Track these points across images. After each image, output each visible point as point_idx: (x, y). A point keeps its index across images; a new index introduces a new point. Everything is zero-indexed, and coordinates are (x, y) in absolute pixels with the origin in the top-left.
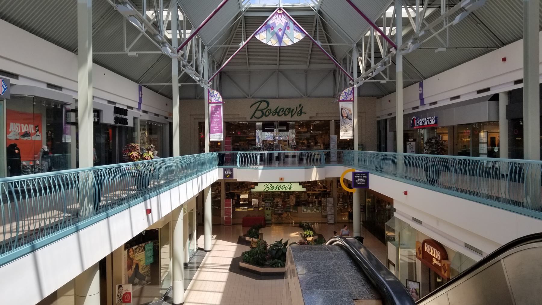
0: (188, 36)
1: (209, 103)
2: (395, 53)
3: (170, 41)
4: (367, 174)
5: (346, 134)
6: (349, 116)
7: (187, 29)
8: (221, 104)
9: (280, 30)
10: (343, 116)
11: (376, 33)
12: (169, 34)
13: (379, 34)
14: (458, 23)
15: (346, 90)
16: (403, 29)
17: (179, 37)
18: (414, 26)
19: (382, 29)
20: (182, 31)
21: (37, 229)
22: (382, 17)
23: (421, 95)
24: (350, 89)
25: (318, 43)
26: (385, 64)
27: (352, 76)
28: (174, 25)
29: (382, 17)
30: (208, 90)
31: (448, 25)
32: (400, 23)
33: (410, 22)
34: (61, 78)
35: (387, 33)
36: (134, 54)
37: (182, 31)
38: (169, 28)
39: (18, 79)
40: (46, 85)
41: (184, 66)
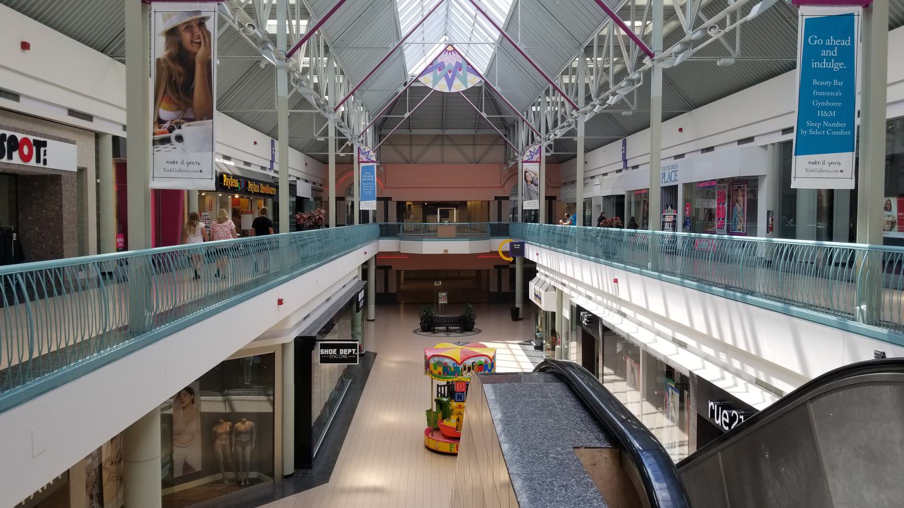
0: (303, 31)
1: (359, 162)
2: (650, 65)
3: (273, 38)
4: (522, 245)
5: (530, 205)
6: (535, 180)
7: (302, 19)
8: (375, 164)
9: (450, 72)
10: (527, 181)
11: (618, 31)
12: (272, 26)
13: (623, 32)
14: (756, 18)
15: (532, 149)
16: (665, 24)
17: (288, 32)
18: (685, 22)
19: (628, 24)
20: (294, 22)
21: (16, 367)
22: (630, 3)
23: (624, 155)
24: (537, 147)
25: (484, 115)
26: (632, 82)
27: (540, 130)
28: (280, 13)
29: (630, 3)
30: (359, 148)
31: (740, 22)
32: (659, 14)
33: (675, 13)
34: (17, 76)
35: (637, 32)
36: (343, 155)
37: (294, 22)
38: (273, 16)
39: (92, 121)
40: (66, 112)
41: (297, 81)
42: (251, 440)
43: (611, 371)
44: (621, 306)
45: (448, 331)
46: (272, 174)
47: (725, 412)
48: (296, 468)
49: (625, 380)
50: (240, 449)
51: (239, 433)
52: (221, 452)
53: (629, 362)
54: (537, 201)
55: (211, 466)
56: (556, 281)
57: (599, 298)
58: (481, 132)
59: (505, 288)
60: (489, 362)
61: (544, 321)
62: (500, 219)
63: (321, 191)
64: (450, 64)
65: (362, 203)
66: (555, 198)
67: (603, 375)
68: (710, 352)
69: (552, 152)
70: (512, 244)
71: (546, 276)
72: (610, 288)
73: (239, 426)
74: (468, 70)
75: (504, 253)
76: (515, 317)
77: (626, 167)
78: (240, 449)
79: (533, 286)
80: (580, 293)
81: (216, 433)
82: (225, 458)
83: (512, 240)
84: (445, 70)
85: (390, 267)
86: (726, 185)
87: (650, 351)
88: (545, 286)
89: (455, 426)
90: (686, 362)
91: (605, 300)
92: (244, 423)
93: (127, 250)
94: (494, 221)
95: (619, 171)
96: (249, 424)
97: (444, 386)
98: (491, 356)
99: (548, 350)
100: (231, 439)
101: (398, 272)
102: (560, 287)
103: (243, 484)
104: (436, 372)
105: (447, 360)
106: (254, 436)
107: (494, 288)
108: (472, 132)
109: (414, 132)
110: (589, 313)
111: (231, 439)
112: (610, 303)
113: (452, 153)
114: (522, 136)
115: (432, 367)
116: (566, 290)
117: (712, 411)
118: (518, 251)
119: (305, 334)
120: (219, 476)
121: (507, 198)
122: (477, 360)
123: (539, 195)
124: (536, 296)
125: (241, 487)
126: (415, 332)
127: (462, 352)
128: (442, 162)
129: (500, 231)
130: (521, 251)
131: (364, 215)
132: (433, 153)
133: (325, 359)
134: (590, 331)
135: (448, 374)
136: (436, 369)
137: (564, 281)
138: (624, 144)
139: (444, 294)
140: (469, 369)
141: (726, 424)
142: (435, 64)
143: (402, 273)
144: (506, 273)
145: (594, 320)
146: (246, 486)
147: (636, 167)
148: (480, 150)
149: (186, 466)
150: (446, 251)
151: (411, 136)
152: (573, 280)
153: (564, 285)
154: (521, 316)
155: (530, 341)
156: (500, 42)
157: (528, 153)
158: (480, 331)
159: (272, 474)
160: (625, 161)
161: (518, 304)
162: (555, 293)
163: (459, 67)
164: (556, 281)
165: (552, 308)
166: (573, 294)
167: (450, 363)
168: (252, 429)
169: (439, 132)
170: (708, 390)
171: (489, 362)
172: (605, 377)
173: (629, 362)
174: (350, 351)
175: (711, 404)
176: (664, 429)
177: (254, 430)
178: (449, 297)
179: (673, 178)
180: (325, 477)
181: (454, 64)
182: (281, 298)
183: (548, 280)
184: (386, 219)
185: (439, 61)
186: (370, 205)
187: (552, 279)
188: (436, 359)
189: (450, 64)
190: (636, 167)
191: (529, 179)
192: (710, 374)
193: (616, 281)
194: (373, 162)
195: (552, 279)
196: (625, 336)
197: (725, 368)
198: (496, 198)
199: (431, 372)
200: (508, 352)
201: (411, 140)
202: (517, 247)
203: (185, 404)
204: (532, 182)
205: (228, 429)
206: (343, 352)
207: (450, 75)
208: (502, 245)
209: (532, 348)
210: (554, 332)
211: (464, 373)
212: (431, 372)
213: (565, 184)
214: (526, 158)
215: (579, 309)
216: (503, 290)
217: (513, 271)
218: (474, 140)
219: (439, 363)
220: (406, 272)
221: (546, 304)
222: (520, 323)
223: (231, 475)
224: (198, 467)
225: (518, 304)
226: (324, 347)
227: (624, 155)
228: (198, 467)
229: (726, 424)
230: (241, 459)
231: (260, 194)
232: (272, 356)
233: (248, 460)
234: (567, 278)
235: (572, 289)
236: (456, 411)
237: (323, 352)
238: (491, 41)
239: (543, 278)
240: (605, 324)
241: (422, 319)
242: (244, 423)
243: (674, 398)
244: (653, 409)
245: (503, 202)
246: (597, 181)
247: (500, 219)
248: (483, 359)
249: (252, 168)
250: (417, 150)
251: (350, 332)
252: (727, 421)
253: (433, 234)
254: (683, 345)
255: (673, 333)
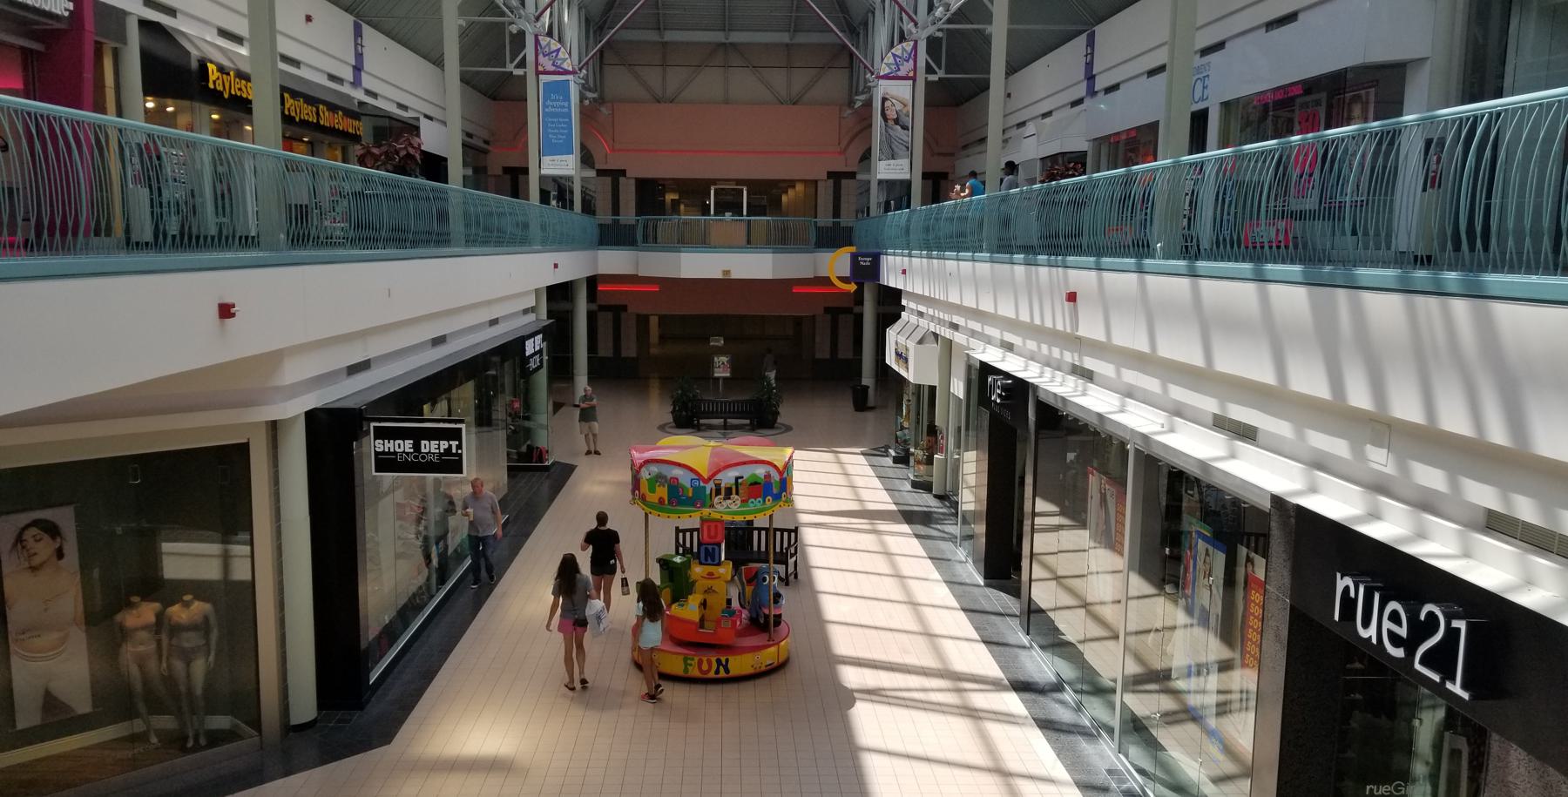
1: (538, 73)
4: (876, 259)
5: (887, 169)
15: (898, 50)
23: (1089, 65)
24: (908, 46)
42: (208, 644)
43: (1052, 508)
44: (1082, 360)
45: (725, 427)
46: (359, 95)
47: (1393, 605)
48: (321, 705)
49: (1083, 525)
50: (179, 665)
51: (176, 630)
52: (134, 670)
53: (1095, 482)
54: (905, 162)
55: (116, 700)
56: (940, 322)
57: (1032, 345)
58: (802, 38)
59: (845, 353)
60: (776, 477)
61: (913, 408)
62: (836, 213)
63: (485, 152)
65: (546, 160)
66: (944, 176)
67: (1034, 514)
68: (1338, 447)
69: (941, 74)
70: (854, 257)
71: (921, 314)
72: (1058, 319)
73: (177, 613)
75: (842, 279)
76: (861, 404)
77: (1092, 92)
78: (179, 665)
79: (892, 335)
80: (988, 340)
81: (122, 628)
82: (145, 682)
83: (853, 249)
85: (624, 308)
86: (1323, 96)
87: (1157, 452)
88: (918, 335)
89: (696, 618)
90: (1262, 474)
91: (1045, 348)
92: (187, 605)
94: (825, 219)
95: (1079, 102)
96: (199, 608)
97: (692, 531)
98: (780, 465)
99: (919, 462)
100: (159, 642)
101: (643, 321)
102: (946, 333)
103: (190, 744)
104: (653, 498)
105: (677, 472)
106: (214, 636)
107: (823, 352)
108: (784, 38)
109: (670, 36)
110: (1007, 375)
111: (159, 642)
112: (1056, 352)
113: (744, 83)
114: (881, 36)
115: (644, 488)
116: (959, 338)
117: (1349, 604)
118: (866, 271)
120: (138, 726)
121: (852, 175)
122: (747, 472)
123: (909, 149)
124: (899, 355)
125: (184, 750)
126: (662, 428)
127: (715, 453)
128: (726, 102)
129: (832, 238)
130: (874, 271)
131: (557, 191)
132: (709, 83)
133: (387, 463)
134: (1007, 415)
135: (679, 503)
136: (652, 490)
137: (956, 319)
138: (1091, 43)
139: (724, 359)
140: (729, 492)
141: (1395, 640)
143: (654, 321)
144: (846, 321)
145: (1019, 389)
146: (197, 748)
147: (1114, 88)
148: (800, 78)
149: (50, 703)
150: (727, 272)
151: (664, 44)
152: (977, 314)
153: (955, 327)
154: (871, 402)
155: (887, 447)
157: (889, 59)
158: (788, 429)
159: (256, 723)
160: (1090, 78)
161: (867, 380)
162: (934, 349)
164: (940, 322)
165: (931, 378)
166: (974, 342)
167: (685, 478)
168: (206, 618)
169: (718, 37)
170: (1324, 545)
171: (776, 477)
172: (1038, 520)
173: (1095, 482)
174: (444, 445)
175: (1343, 582)
176: (1179, 633)
177: (213, 620)
178: (734, 366)
179: (1197, 96)
180: (385, 732)
182: (228, 300)
183: (923, 322)
184: (616, 210)
186: (563, 165)
187: (932, 318)
188: (654, 469)
190: (1114, 88)
191: (892, 114)
192: (1335, 503)
193: (1072, 297)
194: (566, 72)
195: (932, 318)
196: (1094, 421)
197: (1378, 487)
198: (831, 175)
199: (643, 498)
200: (835, 468)
201: (666, 54)
202: (865, 262)
203: (37, 561)
204: (897, 121)
205: (152, 619)
206: (430, 447)
208: (836, 264)
209: (889, 461)
210: (932, 430)
211: (716, 500)
212: (643, 498)
213: (965, 147)
214: (885, 70)
215: (986, 369)
216: (841, 356)
217: (859, 318)
218: (789, 55)
219: (659, 478)
220: (663, 319)
221: (917, 370)
222: (869, 415)
223: (166, 722)
224: (82, 704)
225: (867, 380)
226: (382, 434)
227: (1089, 65)
228: (82, 704)
229: (1395, 640)
230: (183, 688)
231: (332, 131)
232: (243, 450)
233: (199, 691)
234: (965, 311)
235: (973, 334)
236: (701, 585)
237: (382, 446)
239: (914, 319)
240: (1042, 397)
241: (674, 404)
242: (187, 605)
243: (1207, 561)
244: (1148, 589)
245: (844, 182)
246: (1030, 129)
247: (836, 213)
248: (760, 471)
249: (303, 72)
250: (675, 77)
251: (1136, 594)
252: (1403, 632)
253: (701, 241)
254: (1246, 433)
255: (1223, 407)
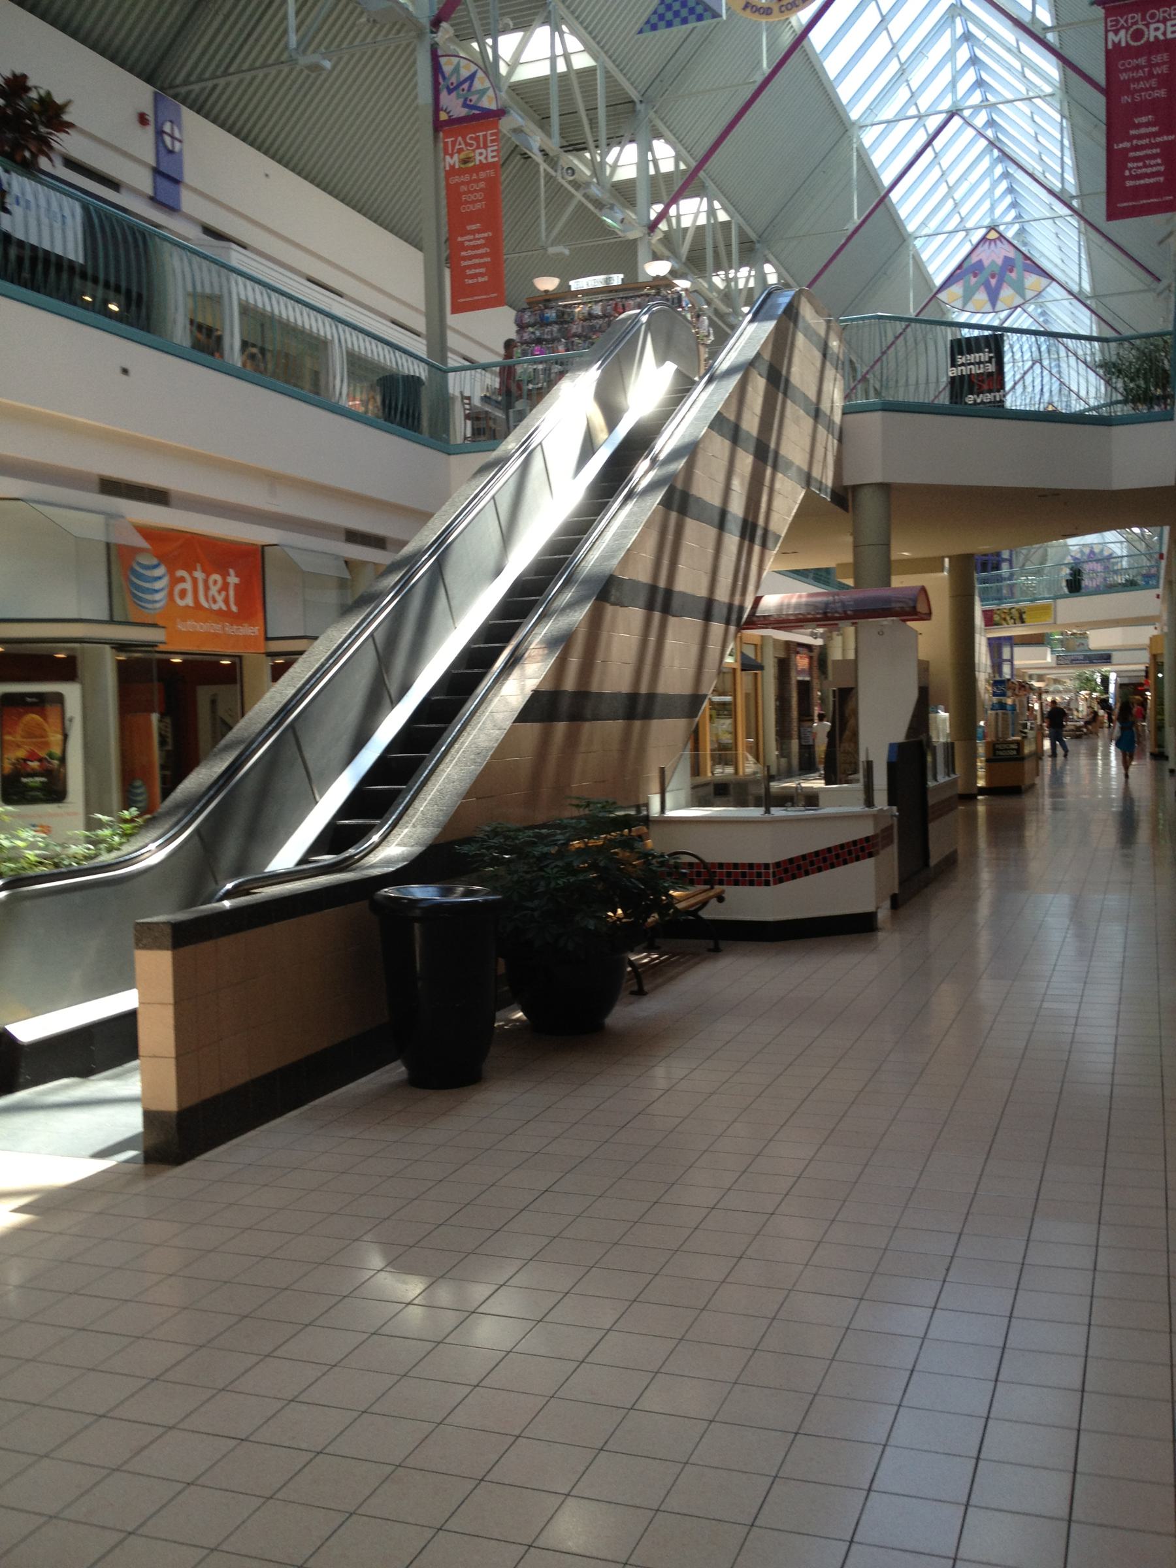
9: (993, 276)
64: (993, 262)
74: (1026, 269)
84: (982, 277)
93: (788, 645)
119: (687, 440)
142: (965, 265)
156: (1066, 84)
163: (1008, 264)
172: (983, 143)
181: (999, 262)
185: (974, 259)
189: (993, 262)
207: (993, 282)
238: (1048, 90)
